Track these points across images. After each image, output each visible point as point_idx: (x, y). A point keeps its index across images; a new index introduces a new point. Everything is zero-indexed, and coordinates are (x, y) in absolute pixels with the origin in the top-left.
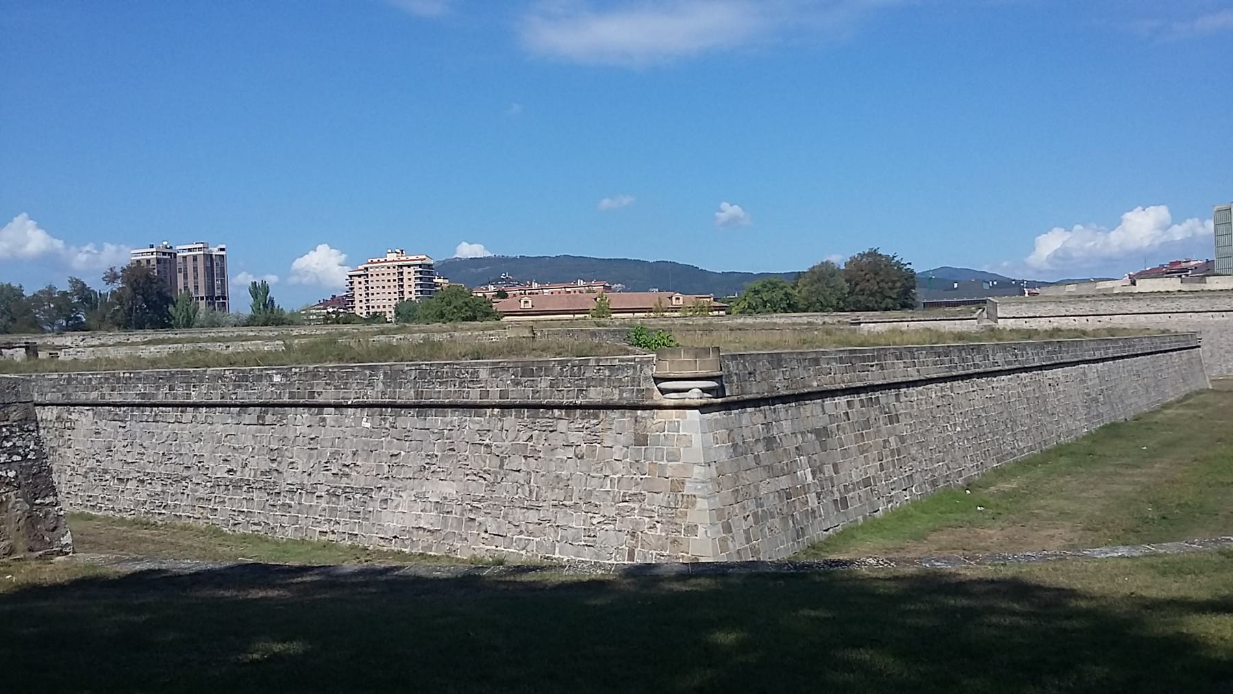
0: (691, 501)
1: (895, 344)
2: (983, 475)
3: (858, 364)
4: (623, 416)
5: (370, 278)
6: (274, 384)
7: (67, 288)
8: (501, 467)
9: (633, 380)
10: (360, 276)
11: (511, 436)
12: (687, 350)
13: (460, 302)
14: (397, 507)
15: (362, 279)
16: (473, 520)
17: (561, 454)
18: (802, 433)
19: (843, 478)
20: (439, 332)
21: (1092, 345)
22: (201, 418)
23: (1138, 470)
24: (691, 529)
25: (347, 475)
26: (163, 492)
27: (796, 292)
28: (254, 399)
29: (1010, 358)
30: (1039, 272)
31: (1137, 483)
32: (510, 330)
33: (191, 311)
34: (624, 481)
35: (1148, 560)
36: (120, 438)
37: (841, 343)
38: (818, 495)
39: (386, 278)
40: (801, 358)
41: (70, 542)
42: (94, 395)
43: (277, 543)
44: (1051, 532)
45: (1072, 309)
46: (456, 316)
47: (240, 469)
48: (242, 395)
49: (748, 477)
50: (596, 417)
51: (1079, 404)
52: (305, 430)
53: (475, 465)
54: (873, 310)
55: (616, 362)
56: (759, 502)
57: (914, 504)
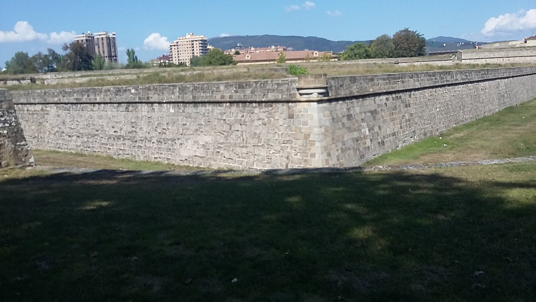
0: (313, 143)
1: (410, 71)
2: (448, 130)
3: (392, 81)
4: (283, 105)
5: (179, 47)
6: (132, 94)
7: (47, 53)
8: (230, 129)
9: (288, 90)
10: (175, 46)
11: (235, 115)
12: (312, 75)
13: (218, 57)
14: (186, 147)
15: (176, 47)
16: (219, 152)
17: (256, 123)
18: (365, 113)
19: (383, 133)
20: (207, 70)
21: (503, 71)
22: (101, 109)
23: (519, 127)
24: (313, 155)
25: (165, 133)
26: (88, 141)
27: (370, 49)
28: (124, 100)
29: (464, 77)
30: (486, 37)
31: (518, 133)
32: (241, 68)
33: (101, 63)
34: (284, 135)
35: (506, 165)
36: (68, 118)
37: (385, 71)
38: (371, 140)
39: (186, 46)
40: (365, 78)
41: (33, 161)
42: (56, 100)
43: (136, 162)
44: (476, 155)
45: (496, 55)
46: (216, 63)
47: (119, 131)
48: (118, 99)
49: (339, 132)
50: (271, 106)
51: (495, 98)
52: (146, 113)
53: (219, 128)
54: (403, 56)
55: (280, 82)
56: (344, 143)
57: (415, 143)
